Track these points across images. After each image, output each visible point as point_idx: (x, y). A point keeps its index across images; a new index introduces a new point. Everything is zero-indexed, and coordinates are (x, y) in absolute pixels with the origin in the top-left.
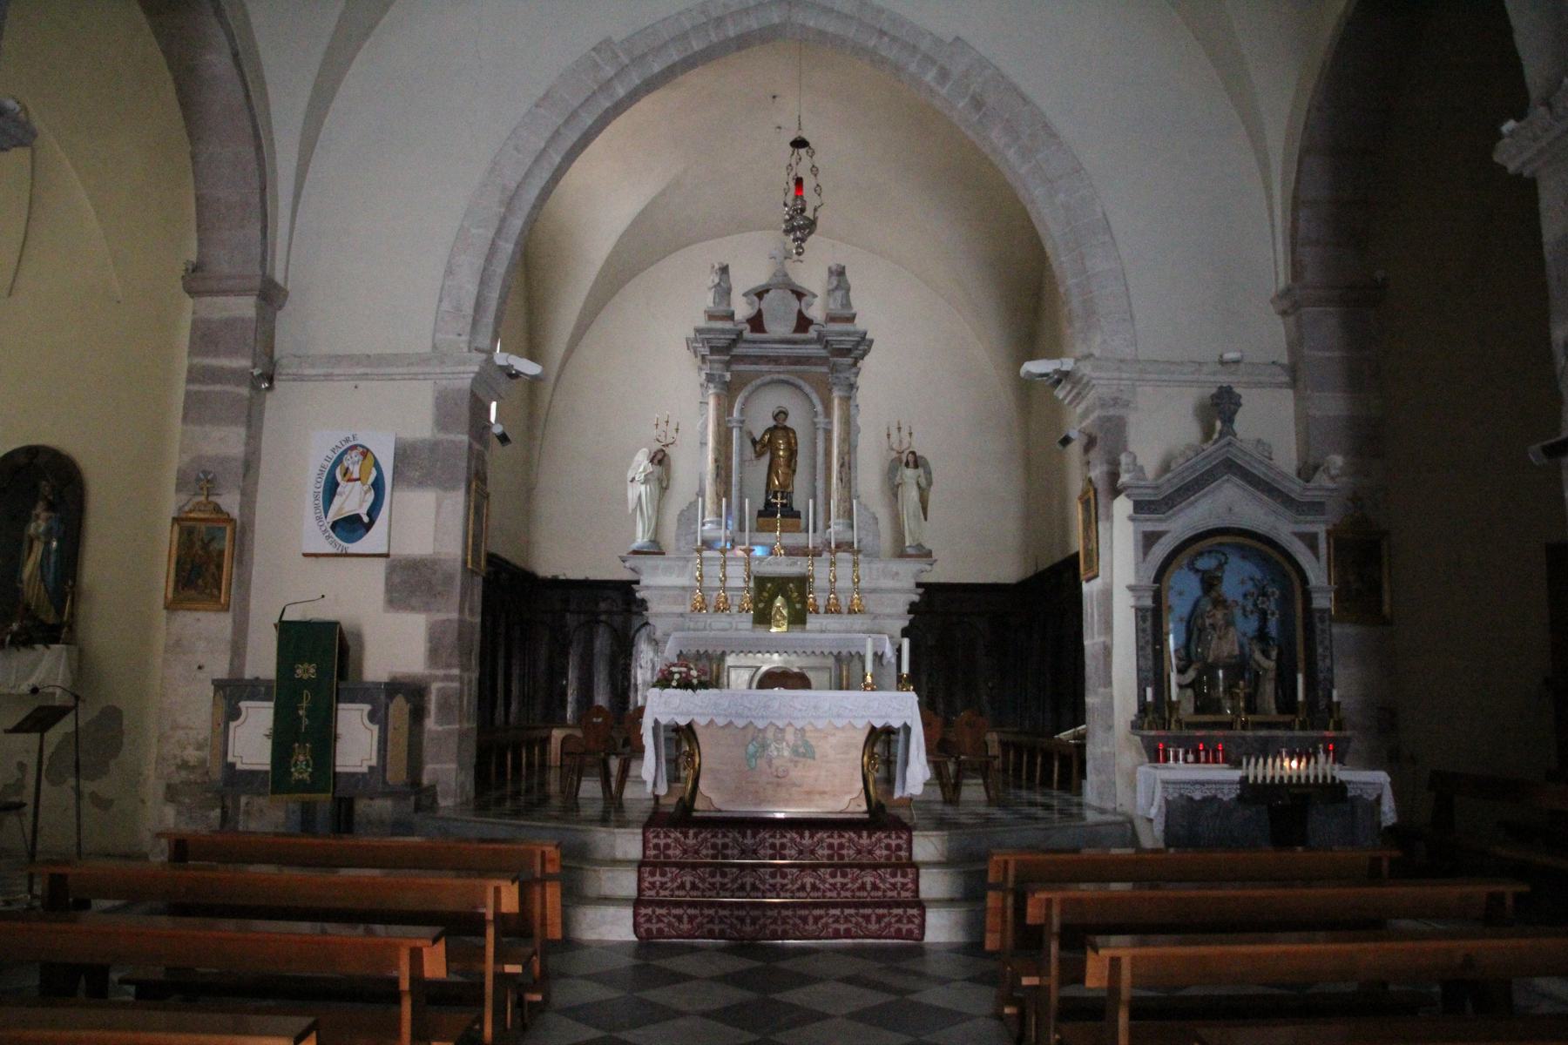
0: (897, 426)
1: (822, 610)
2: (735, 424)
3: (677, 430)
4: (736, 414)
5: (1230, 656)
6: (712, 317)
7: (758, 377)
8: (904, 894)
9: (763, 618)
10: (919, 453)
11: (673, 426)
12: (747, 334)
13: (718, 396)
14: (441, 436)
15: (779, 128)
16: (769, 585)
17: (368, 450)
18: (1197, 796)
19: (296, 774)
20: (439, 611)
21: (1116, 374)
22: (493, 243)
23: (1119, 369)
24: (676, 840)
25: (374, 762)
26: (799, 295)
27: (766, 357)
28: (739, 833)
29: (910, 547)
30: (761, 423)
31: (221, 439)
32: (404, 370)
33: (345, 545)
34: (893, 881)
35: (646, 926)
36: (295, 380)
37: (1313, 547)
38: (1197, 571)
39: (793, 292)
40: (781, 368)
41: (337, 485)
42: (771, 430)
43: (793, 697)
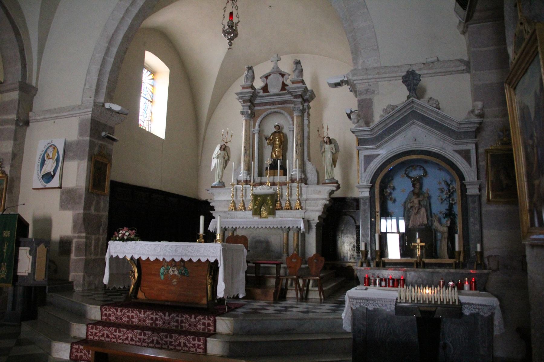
0: (327, 128)
1: (293, 208)
2: (256, 132)
3: (232, 136)
4: (257, 127)
5: (422, 225)
6: (244, 88)
7: (266, 111)
8: (199, 350)
9: (257, 212)
10: (331, 138)
11: (230, 134)
12: (261, 93)
13: (246, 120)
14: (81, 138)
15: (270, 6)
16: (259, 198)
17: (56, 146)
18: (371, 308)
19: (2, 275)
20: (76, 210)
21: (365, 77)
22: (104, 59)
23: (366, 74)
24: (113, 312)
25: (30, 271)
26: (283, 75)
27: (269, 102)
28: (138, 311)
29: (327, 179)
30: (270, 130)
31: (6, 146)
32: (67, 113)
33: (46, 184)
34: (193, 342)
35: (76, 354)
36: (36, 122)
37: (468, 159)
38: (411, 178)
39: (280, 74)
40: (275, 107)
41: (45, 160)
42: (274, 134)
43: (188, 246)
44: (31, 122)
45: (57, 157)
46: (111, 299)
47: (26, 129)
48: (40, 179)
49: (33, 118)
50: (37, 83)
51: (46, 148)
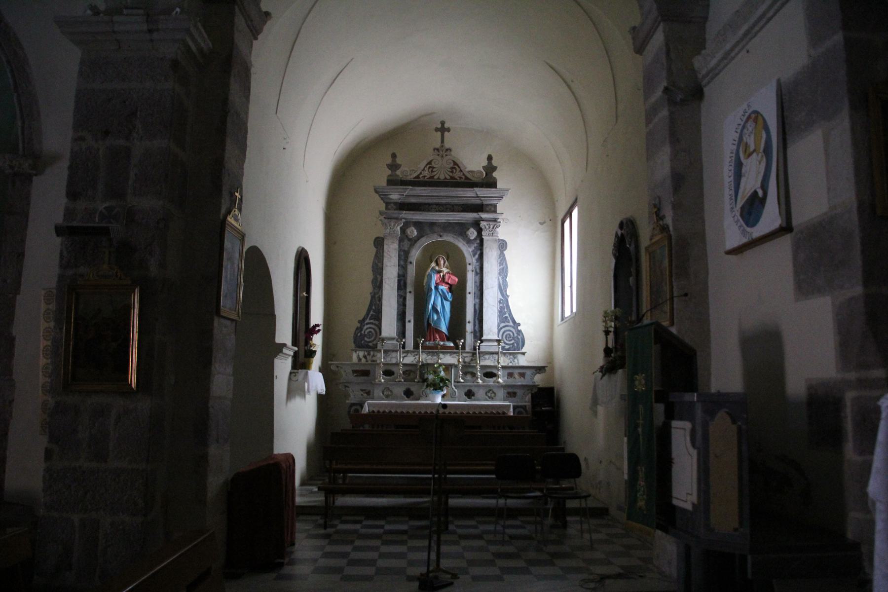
44: (705, 86)
45: (766, 138)
46: (533, 569)
48: (737, 222)
49: (704, 72)
51: (739, 131)
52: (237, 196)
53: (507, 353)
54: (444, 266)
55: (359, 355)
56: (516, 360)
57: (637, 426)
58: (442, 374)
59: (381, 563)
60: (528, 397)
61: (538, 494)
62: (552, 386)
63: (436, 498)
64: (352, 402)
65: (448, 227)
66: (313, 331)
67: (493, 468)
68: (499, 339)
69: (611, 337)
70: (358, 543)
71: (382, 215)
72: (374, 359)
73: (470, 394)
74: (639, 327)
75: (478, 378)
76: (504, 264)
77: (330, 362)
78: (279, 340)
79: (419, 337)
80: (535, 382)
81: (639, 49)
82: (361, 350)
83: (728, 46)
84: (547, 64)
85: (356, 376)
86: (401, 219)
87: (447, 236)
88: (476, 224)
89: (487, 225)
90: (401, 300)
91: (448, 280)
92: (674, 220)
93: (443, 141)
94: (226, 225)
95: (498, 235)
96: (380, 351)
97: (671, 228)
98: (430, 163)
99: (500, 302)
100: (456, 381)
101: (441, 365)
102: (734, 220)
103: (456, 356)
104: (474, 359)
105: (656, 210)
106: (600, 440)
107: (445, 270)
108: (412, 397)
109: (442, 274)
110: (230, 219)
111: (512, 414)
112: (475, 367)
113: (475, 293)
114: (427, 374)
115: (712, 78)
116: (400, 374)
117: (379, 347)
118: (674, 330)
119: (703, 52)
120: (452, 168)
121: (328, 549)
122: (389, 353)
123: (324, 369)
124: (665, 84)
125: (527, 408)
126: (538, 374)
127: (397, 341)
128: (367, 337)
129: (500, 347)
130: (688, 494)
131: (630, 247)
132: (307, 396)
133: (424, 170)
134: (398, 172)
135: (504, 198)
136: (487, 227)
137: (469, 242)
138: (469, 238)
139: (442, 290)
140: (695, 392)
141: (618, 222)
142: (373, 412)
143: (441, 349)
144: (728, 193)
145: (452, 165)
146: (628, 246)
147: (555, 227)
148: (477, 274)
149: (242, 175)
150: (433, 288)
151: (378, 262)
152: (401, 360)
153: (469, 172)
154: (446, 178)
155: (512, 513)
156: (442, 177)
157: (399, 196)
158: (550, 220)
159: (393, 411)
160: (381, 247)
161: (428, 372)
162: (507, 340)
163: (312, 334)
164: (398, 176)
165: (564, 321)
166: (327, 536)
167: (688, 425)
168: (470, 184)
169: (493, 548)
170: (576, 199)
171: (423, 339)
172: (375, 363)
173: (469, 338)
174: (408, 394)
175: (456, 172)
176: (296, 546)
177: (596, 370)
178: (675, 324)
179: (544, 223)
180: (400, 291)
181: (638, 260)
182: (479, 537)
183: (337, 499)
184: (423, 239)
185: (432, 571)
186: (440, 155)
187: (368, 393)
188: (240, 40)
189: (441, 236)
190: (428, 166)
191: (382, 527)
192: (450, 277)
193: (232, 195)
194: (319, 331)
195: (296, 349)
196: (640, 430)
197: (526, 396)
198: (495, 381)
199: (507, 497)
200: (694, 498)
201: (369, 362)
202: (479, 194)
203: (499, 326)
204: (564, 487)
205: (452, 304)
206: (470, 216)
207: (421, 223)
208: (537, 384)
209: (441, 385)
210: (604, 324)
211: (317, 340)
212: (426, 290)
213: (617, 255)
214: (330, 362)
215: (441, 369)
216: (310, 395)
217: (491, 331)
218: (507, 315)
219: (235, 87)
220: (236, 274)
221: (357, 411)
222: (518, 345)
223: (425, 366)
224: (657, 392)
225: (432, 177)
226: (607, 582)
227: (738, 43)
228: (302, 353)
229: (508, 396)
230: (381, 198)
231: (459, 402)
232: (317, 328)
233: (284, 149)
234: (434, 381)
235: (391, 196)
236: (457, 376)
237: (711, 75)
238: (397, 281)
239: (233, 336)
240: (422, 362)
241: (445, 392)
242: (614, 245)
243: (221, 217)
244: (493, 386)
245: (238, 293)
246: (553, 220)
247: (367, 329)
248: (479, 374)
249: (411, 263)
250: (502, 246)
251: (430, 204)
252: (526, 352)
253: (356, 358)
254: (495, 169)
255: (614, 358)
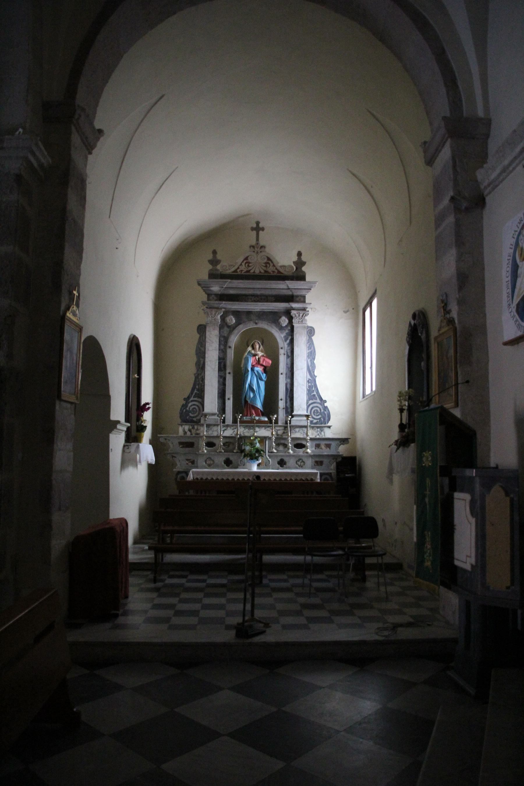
44: (487, 195)
47: (482, 213)
48: (514, 317)
49: (486, 183)
50: (487, 108)
51: (516, 237)
52: (75, 294)
53: (315, 426)
54: (259, 350)
55: (184, 429)
56: (323, 433)
57: (424, 496)
58: (258, 445)
59: (204, 613)
60: (333, 466)
61: (340, 552)
62: (354, 455)
63: (250, 555)
64: (178, 470)
65: (262, 315)
66: (143, 408)
67: (302, 528)
68: (307, 414)
69: (405, 414)
70: (184, 595)
71: (204, 305)
72: (198, 432)
73: (282, 463)
74: (427, 411)
75: (289, 449)
76: (312, 348)
77: (159, 435)
78: (113, 417)
79: (237, 413)
80: (339, 452)
81: (430, 162)
82: (186, 425)
83: (506, 162)
84: (350, 171)
85: (181, 447)
86: (221, 308)
87: (262, 323)
88: (288, 313)
89: (297, 313)
90: (221, 380)
91: (263, 362)
92: (459, 314)
93: (257, 239)
94: (66, 320)
95: (307, 323)
96: (203, 425)
97: (456, 321)
98: (246, 258)
99: (308, 382)
100: (270, 451)
101: (256, 437)
102: (511, 315)
103: (270, 430)
104: (285, 431)
105: (443, 305)
106: (396, 505)
107: (260, 354)
108: (231, 465)
109: (257, 357)
110: (69, 315)
111: (319, 481)
112: (286, 439)
113: (286, 374)
114: (244, 446)
115: (493, 189)
116: (221, 445)
117: (202, 421)
118: (457, 413)
119: (485, 165)
120: (266, 263)
121: (157, 601)
122: (211, 427)
123: (153, 442)
124: (451, 193)
125: (333, 475)
126: (342, 445)
127: (218, 416)
128: (192, 413)
129: (309, 421)
130: (467, 556)
131: (421, 335)
132: (139, 466)
133: (241, 265)
134: (219, 267)
135: (312, 290)
136: (297, 315)
137: (281, 328)
138: (281, 325)
139: (257, 372)
140: (474, 468)
141: (412, 313)
142: (197, 479)
143: (256, 423)
144: (506, 291)
145: (266, 260)
146: (420, 335)
147: (358, 315)
148: (288, 357)
149: (79, 275)
150: (250, 369)
151: (201, 346)
152: (222, 433)
153: (281, 267)
154: (260, 272)
155: (319, 568)
156: (257, 272)
157: (219, 288)
158: (353, 309)
159: (214, 478)
160: (203, 333)
161: (245, 444)
162: (314, 415)
163: (143, 412)
164: (219, 270)
165: (365, 398)
166: (157, 590)
167: (467, 497)
168: (282, 277)
169: (302, 600)
170: (376, 291)
171: (241, 415)
172: (198, 436)
173: (282, 414)
174: (228, 463)
175: (269, 267)
176: (130, 599)
177: (391, 444)
178: (459, 406)
179: (348, 311)
180: (220, 372)
181: (428, 347)
182: (287, 590)
183: (165, 557)
184: (241, 326)
185: (247, 621)
186: (256, 251)
187: (193, 462)
188: (76, 156)
189: (256, 324)
190: (245, 261)
191: (204, 581)
192: (264, 360)
193: (71, 293)
194: (149, 408)
195: (129, 425)
196: (427, 500)
197: (331, 465)
198: (304, 451)
199: (313, 555)
200: (473, 560)
201: (194, 435)
202: (291, 286)
203: (307, 403)
204: (363, 546)
205: (266, 383)
206: (282, 306)
207: (238, 312)
208: (341, 454)
209: (257, 455)
210: (399, 403)
211: (148, 416)
212: (243, 372)
213: (410, 342)
214: (159, 435)
215: (257, 441)
216: (141, 465)
217: (300, 407)
218: (315, 393)
219: (68, 253)
220: (75, 362)
221: (183, 478)
222: (324, 419)
223: (243, 438)
224: (441, 467)
225: (248, 271)
226: (400, 629)
227: (515, 158)
228: (134, 428)
229: (315, 464)
230: (203, 290)
231: (274, 470)
232: (147, 406)
233: (117, 248)
234: (250, 451)
235: (212, 289)
236: (271, 447)
237: (492, 186)
238: (217, 363)
239: (73, 416)
240: (240, 435)
241: (260, 461)
242: (408, 334)
243: (61, 313)
244: (302, 456)
245: (76, 377)
246: (355, 309)
247: (191, 406)
248: (290, 445)
249: (230, 347)
250: (310, 332)
251: (246, 295)
252: (331, 426)
253: (182, 432)
254: (304, 264)
255: (408, 432)
